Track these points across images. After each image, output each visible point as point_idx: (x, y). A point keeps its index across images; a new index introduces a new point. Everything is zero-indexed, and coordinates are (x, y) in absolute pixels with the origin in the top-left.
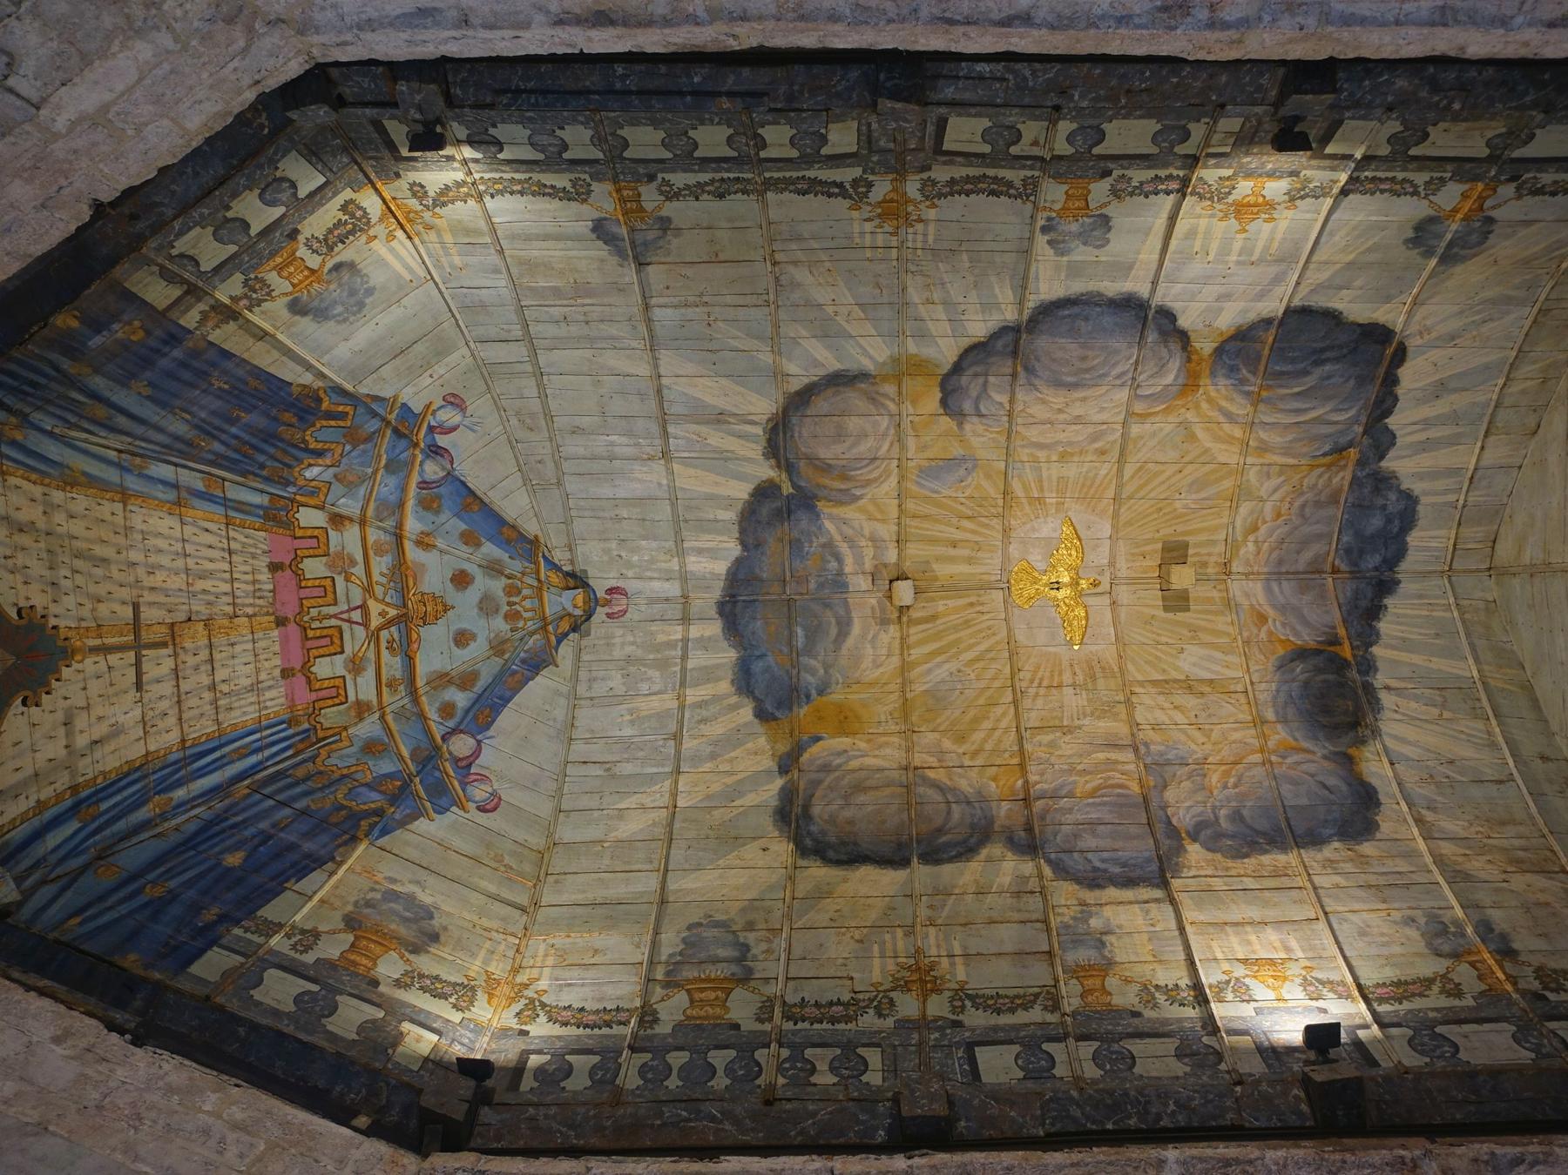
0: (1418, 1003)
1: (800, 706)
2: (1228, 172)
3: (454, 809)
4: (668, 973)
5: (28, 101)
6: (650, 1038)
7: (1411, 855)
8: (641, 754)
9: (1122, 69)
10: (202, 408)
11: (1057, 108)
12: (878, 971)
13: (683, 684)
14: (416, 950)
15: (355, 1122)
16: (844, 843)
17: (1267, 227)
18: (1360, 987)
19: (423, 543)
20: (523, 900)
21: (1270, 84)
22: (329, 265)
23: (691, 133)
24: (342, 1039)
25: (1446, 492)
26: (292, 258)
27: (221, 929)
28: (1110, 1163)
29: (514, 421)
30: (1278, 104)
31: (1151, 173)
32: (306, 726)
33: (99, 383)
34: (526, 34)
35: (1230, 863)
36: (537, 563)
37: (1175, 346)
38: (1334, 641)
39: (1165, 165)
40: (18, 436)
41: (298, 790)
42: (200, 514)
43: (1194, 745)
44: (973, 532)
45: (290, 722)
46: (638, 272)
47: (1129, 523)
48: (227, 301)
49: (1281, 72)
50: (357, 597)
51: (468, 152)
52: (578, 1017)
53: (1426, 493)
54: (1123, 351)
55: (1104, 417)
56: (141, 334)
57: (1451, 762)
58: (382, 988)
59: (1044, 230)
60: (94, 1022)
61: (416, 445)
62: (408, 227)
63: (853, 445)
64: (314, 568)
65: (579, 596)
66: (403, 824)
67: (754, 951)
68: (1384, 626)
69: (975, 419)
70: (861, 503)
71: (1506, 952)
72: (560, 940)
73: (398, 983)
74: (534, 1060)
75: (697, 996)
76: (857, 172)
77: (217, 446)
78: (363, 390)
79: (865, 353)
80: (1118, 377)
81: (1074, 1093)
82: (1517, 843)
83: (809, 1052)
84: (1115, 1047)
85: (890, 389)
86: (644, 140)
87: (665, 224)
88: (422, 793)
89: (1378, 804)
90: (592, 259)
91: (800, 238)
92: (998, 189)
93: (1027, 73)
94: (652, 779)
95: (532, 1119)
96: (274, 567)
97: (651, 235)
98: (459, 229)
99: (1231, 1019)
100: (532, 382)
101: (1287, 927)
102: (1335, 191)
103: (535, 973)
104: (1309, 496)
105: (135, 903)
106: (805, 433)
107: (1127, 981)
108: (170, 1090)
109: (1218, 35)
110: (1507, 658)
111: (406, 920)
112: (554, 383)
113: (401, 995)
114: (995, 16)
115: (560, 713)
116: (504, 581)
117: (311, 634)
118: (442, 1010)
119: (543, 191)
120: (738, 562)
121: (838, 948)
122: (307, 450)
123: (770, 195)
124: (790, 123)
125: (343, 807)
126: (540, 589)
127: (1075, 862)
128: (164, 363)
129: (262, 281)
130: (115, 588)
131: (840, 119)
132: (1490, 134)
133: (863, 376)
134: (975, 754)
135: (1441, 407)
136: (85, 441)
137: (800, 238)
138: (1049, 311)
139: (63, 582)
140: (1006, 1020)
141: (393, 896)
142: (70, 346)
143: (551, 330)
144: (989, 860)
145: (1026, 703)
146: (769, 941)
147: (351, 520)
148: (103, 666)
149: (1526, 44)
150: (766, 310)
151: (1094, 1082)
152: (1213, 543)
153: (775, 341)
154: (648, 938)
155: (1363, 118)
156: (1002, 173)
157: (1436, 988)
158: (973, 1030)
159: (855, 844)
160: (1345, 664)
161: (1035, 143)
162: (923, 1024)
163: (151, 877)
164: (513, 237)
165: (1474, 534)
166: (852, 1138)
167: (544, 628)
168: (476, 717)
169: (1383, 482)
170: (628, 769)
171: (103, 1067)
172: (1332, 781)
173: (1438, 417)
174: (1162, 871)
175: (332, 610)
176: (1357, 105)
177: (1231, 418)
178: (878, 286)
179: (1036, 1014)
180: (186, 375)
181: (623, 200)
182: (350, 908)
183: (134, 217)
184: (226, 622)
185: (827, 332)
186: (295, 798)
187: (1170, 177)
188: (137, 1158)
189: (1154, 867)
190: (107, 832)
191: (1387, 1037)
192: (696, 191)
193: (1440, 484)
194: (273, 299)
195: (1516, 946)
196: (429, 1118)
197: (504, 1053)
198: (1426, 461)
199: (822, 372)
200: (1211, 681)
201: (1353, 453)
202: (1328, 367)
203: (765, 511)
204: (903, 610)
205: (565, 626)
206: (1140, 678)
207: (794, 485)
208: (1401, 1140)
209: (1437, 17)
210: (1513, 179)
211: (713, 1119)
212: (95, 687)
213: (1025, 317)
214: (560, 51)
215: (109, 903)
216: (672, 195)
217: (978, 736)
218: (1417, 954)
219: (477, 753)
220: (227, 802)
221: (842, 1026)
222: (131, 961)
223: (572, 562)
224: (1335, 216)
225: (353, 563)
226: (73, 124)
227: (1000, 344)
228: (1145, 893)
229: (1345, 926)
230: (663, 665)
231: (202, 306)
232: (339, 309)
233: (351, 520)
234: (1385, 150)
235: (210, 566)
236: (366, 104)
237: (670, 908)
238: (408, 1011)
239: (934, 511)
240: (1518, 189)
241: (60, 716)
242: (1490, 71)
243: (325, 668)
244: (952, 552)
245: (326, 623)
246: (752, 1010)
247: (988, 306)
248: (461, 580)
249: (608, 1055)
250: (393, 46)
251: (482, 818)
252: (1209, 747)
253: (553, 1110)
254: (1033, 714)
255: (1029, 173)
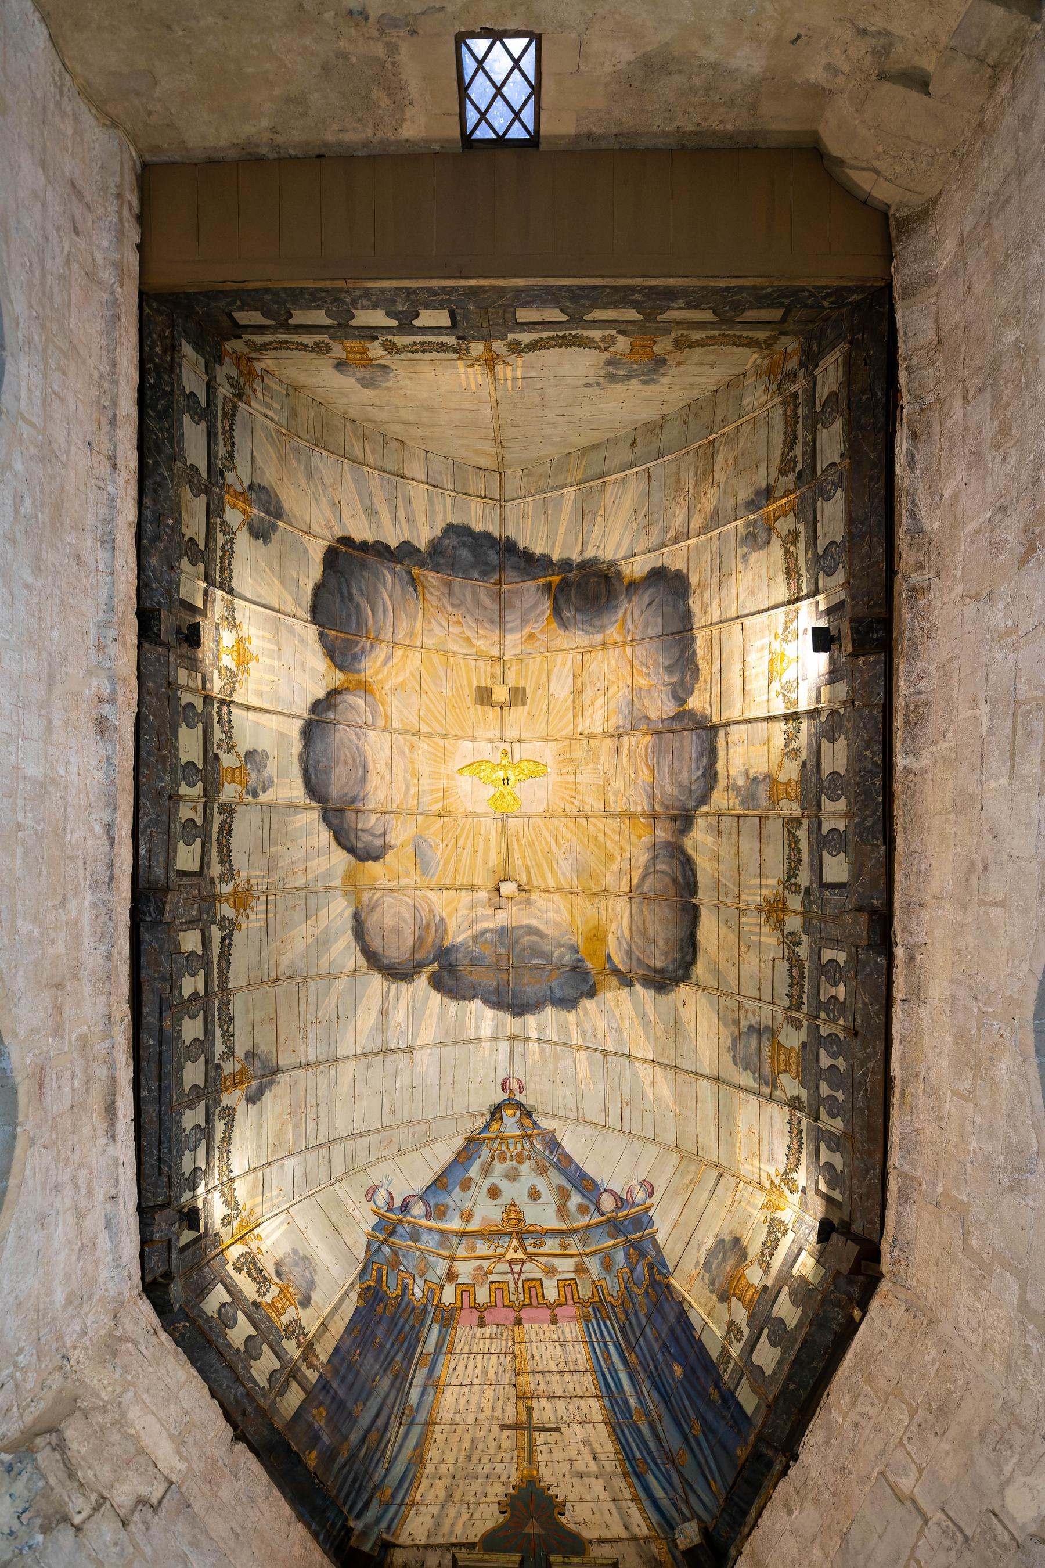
0: (802, 562)
1: (585, 967)
2: (216, 673)
3: (650, 1213)
4: (767, 1084)
5: (167, 1491)
6: (810, 1105)
7: (699, 550)
8: (617, 1080)
9: (143, 755)
10: (372, 1367)
11: (170, 797)
12: (769, 939)
13: (569, 1046)
14: (744, 1255)
15: (857, 1319)
16: (681, 949)
17: (254, 641)
18: (790, 602)
19: (468, 1218)
20: (714, 1174)
21: (153, 652)
22: (277, 1280)
23: (187, 1043)
24: (801, 1319)
25: (444, 505)
26: (272, 1305)
27: (724, 1388)
28: (905, 805)
29: (385, 1153)
30: (168, 647)
31: (216, 726)
32: (590, 1309)
33: (354, 1438)
34: (121, 1159)
35: (702, 679)
36: (484, 1139)
37: (338, 699)
38: (548, 587)
39: (211, 717)
40: (390, 1491)
41: (634, 1320)
42: (444, 1372)
43: (619, 694)
44: (467, 838)
45: (588, 1321)
46: (283, 1071)
47: (463, 729)
48: (301, 1350)
49: (146, 645)
50: (503, 1267)
51: (201, 1190)
52: (794, 1151)
53: (445, 518)
54: (341, 736)
55: (387, 747)
56: (321, 1409)
57: (635, 512)
58: (769, 1284)
59: (255, 795)
60: (780, 1484)
61: (401, 1221)
62: (252, 1226)
63: (405, 922)
64: (483, 1295)
65: (507, 1112)
66: (659, 1251)
67: (753, 1022)
68: (538, 550)
69: (388, 837)
70: (445, 916)
71: (768, 493)
72: (742, 1154)
73: (766, 1272)
74: (822, 1187)
75: (782, 1068)
76: (214, 928)
77: (399, 1358)
78: (362, 1257)
79: (341, 914)
80: (359, 738)
81: (856, 820)
82: (692, 473)
83: (823, 998)
84: (826, 784)
85: (365, 896)
86: (193, 1074)
87: (250, 1055)
88: (640, 1234)
89: (663, 568)
90: (275, 1101)
91: (260, 963)
92: (226, 830)
93: (146, 819)
94: (634, 1074)
95: (861, 1196)
96: (481, 1323)
97: (258, 1064)
98: (252, 1193)
99: (809, 698)
100: (358, 1140)
101: (747, 646)
102: (229, 597)
103: (764, 1175)
104: (445, 601)
105: (704, 1444)
106: (396, 955)
107: (781, 766)
108: (827, 1443)
109: (120, 697)
110: (562, 464)
111: (724, 1259)
112: (359, 1126)
113: (774, 1271)
114: (107, 848)
115: (588, 1131)
116: (495, 1162)
117: (527, 1301)
118: (785, 1244)
119: (227, 1138)
120: (485, 1001)
121: (754, 965)
122: (402, 1296)
123: (230, 986)
124: (180, 977)
125: (646, 1291)
126: (502, 1138)
127: (698, 788)
128: (341, 1393)
129: (287, 1326)
130: (492, 1436)
131: (177, 944)
132: (190, 496)
133: (356, 915)
134: (621, 848)
135: (383, 510)
136: (393, 1447)
137: (260, 963)
138: (314, 788)
139: (486, 1471)
140: (805, 856)
141: (707, 1264)
142: (329, 1456)
143: (323, 1129)
144: (695, 849)
145: (587, 809)
146: (746, 1011)
147: (451, 1267)
148: (543, 1448)
149: (127, 481)
150: (310, 984)
151: (849, 804)
152: (477, 668)
153: (331, 977)
154: (743, 1095)
155: (178, 586)
156: (215, 829)
157: (792, 549)
158: (812, 881)
159: (682, 940)
160: (564, 581)
161: (195, 809)
162: (806, 914)
163: (687, 1430)
164: (259, 1156)
165: (475, 484)
166: (882, 980)
167: (529, 1137)
168: (589, 1191)
169: (436, 549)
170: (626, 1090)
171: (810, 1484)
172: (646, 599)
173: (390, 512)
174: (706, 728)
175: (512, 1285)
176: (169, 592)
177: (389, 658)
178: (293, 907)
179: (802, 834)
180: (350, 1378)
181: (234, 1085)
182: (714, 1296)
183: (244, 1413)
184: (517, 1361)
185: (325, 941)
186: (639, 1323)
187: (219, 713)
188: (868, 1478)
189: (703, 733)
190: (656, 1454)
191: (824, 591)
192: (227, 1036)
193: (438, 508)
194: (299, 1319)
195: (764, 486)
196: (855, 1269)
197: (817, 1209)
198: (421, 519)
199: (353, 943)
200: (574, 676)
201: (415, 571)
202: (354, 591)
203: (448, 981)
204: (520, 889)
205: (527, 1122)
206: (571, 727)
207: (432, 962)
208: (896, 595)
209: (108, 546)
210: (222, 474)
211: (865, 1074)
212: (558, 1455)
213: (316, 805)
214: (132, 1134)
215: (703, 1461)
216: (230, 1052)
217: (610, 845)
218: (768, 558)
219: (613, 1193)
220: (639, 1369)
221: (806, 971)
222: (742, 1453)
223: (483, 1115)
224: (247, 595)
225: (480, 1267)
226: (182, 1458)
227: (335, 821)
228: (721, 743)
229: (747, 604)
230: (554, 1056)
231: (304, 1367)
232: (307, 1273)
233: (451, 1267)
234: (201, 567)
235: (479, 1367)
236: (169, 1257)
237: (722, 1075)
238: (785, 1269)
239: (451, 867)
240: (229, 470)
241: (576, 1480)
242: (147, 501)
243: (551, 1293)
244: (480, 853)
245: (520, 1290)
246: (792, 1030)
247: (308, 831)
248: (494, 1192)
249: (820, 1136)
250: (130, 1244)
251: (657, 1196)
252: (621, 684)
253: (855, 1182)
254: (595, 805)
255: (216, 810)
